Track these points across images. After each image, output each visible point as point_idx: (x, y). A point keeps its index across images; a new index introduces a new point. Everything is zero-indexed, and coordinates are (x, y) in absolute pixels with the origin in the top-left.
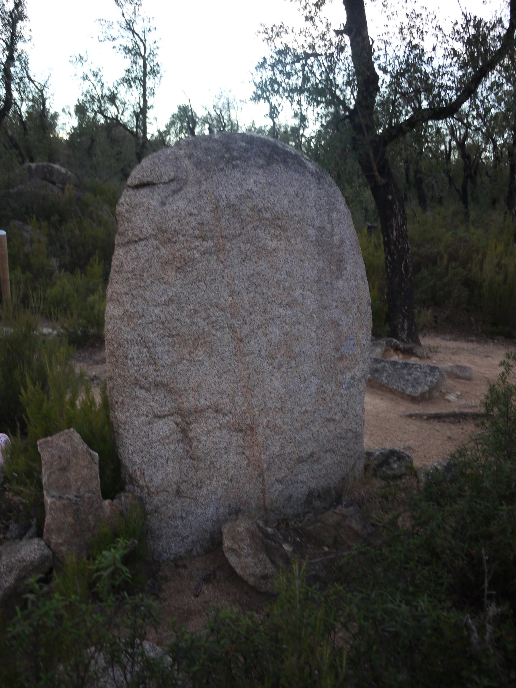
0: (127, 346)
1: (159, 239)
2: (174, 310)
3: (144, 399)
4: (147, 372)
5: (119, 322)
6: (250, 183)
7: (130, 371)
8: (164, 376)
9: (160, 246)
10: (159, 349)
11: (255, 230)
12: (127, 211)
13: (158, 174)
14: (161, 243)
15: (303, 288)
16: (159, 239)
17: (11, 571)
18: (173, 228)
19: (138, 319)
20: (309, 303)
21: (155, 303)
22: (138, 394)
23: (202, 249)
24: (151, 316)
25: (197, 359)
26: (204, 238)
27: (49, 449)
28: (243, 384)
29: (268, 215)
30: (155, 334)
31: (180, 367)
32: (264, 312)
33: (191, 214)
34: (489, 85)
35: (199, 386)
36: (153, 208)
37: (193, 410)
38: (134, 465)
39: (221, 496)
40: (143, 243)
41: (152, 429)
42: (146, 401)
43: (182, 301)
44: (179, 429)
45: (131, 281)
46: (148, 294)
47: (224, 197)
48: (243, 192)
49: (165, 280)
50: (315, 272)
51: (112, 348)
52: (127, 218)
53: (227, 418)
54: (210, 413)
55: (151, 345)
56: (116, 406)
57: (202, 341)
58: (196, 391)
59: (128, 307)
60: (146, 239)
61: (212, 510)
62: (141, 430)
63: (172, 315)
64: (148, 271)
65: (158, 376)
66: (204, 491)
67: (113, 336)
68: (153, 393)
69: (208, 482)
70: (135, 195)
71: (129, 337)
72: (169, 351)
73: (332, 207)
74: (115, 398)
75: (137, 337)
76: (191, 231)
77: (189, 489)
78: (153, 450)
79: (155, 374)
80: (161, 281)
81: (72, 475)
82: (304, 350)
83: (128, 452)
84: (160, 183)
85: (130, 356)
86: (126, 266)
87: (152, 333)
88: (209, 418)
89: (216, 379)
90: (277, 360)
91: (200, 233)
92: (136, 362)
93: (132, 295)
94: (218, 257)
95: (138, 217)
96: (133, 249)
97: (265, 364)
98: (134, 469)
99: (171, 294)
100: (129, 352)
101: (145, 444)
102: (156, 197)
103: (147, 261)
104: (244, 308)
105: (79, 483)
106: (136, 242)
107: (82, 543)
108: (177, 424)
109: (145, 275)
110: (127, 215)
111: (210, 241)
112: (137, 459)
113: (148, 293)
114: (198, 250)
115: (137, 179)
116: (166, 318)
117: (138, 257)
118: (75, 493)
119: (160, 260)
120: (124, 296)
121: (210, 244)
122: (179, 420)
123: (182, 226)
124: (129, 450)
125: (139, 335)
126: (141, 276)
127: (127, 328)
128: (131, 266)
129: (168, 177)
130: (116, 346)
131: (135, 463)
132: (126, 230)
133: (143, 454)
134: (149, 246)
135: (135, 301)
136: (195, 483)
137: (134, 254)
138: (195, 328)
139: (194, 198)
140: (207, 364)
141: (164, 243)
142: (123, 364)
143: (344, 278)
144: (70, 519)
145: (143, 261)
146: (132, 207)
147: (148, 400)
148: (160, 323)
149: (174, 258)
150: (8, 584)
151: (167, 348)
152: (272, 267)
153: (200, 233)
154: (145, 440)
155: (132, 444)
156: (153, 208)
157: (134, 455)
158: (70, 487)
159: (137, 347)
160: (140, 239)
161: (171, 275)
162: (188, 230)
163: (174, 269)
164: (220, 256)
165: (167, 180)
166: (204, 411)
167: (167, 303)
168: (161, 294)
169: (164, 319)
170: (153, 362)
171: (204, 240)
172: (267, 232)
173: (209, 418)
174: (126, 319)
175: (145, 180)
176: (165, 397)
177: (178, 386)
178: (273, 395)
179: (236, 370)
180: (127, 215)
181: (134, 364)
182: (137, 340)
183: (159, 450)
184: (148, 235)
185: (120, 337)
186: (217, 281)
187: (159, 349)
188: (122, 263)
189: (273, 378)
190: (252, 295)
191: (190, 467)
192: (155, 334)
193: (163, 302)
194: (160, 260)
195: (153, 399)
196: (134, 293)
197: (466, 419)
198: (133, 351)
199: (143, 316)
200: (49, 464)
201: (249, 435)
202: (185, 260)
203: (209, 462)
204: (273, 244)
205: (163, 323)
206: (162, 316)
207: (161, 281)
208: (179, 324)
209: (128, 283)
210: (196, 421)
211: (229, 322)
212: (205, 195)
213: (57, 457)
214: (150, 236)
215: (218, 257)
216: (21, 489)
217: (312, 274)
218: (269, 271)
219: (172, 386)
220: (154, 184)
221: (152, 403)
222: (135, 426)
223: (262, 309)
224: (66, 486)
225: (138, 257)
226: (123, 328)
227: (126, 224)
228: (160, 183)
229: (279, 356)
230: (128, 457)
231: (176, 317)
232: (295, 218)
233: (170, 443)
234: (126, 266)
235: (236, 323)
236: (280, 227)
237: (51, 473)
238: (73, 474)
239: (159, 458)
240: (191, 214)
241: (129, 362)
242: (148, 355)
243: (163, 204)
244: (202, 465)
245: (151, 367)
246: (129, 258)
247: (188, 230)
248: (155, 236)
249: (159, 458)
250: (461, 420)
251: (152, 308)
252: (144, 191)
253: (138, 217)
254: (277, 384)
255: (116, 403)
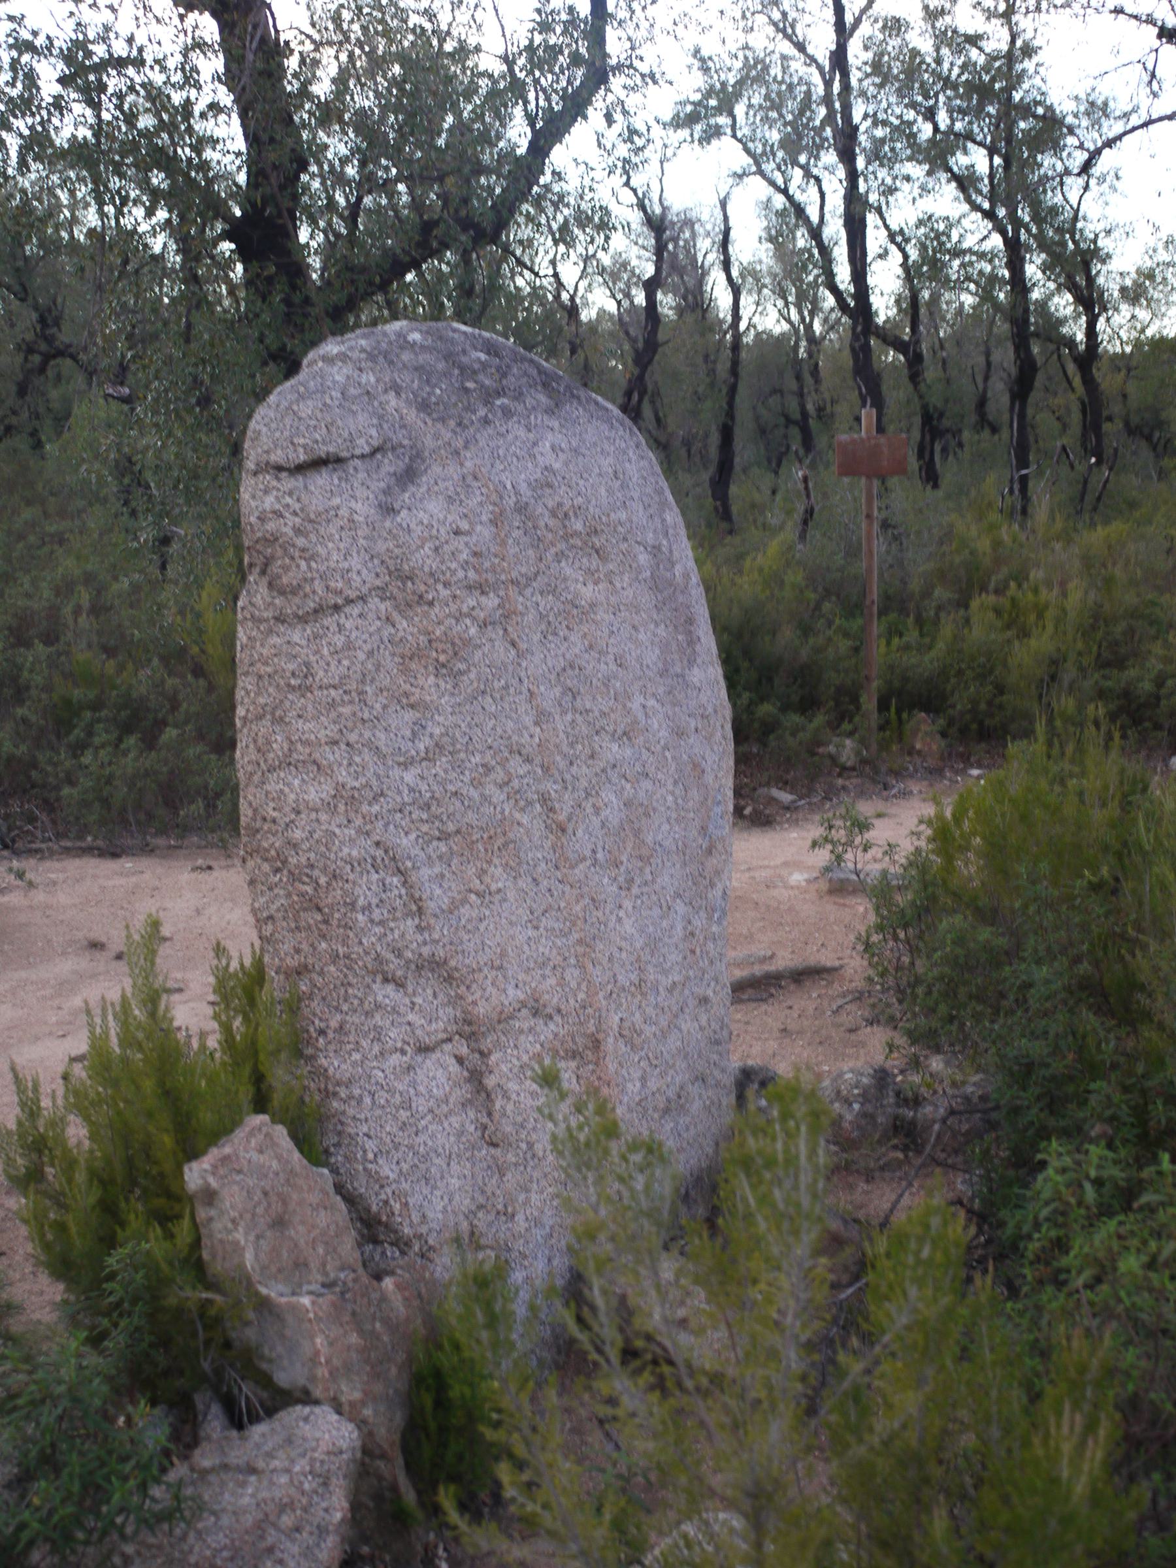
0: (351, 877)
1: (393, 598)
2: (446, 771)
3: (394, 1009)
4: (403, 935)
5: (323, 817)
6: (545, 456)
7: (364, 941)
8: (437, 942)
9: (396, 616)
10: (425, 872)
11: (559, 562)
12: (298, 531)
13: (346, 434)
14: (396, 607)
15: (643, 691)
16: (393, 598)
17: (325, 1484)
18: (426, 569)
19: (370, 804)
20: (656, 726)
21: (402, 759)
22: (380, 998)
23: (482, 615)
24: (399, 792)
25: (494, 887)
26: (482, 588)
27: (238, 1178)
28: (576, 936)
29: (578, 526)
30: (413, 836)
31: (465, 911)
32: (592, 757)
33: (457, 532)
34: (232, 97)
35: (503, 955)
36: (361, 519)
37: (495, 1016)
38: (382, 1187)
39: (552, 1227)
40: (355, 610)
41: (414, 1084)
42: (399, 1014)
43: (458, 746)
44: (466, 1074)
45: (341, 709)
46: (382, 738)
47: (509, 486)
48: (539, 471)
49: (412, 699)
50: (657, 651)
51: (309, 889)
52: (303, 550)
53: (552, 1026)
54: (525, 1021)
55: (409, 864)
56: (321, 1040)
57: (499, 842)
58: (501, 968)
59: (342, 775)
60: (362, 598)
61: (540, 1266)
62: (391, 1091)
63: (442, 783)
64: (373, 680)
65: (425, 943)
66: (520, 1223)
67: (312, 855)
68: (410, 990)
69: (522, 1197)
70: (306, 487)
71: (355, 853)
72: (442, 876)
73: (663, 505)
74: (317, 1022)
75: (372, 851)
76: (461, 574)
77: (490, 1224)
78: (421, 1139)
79: (420, 938)
80: (404, 701)
81: (298, 1232)
82: (660, 837)
83: (365, 1159)
84: (353, 456)
85: (361, 902)
86: (321, 673)
87: (406, 834)
88: (521, 1031)
89: (531, 933)
90: (622, 869)
91: (477, 577)
92: (377, 915)
93: (348, 744)
94: (505, 630)
95: (330, 545)
96: (334, 628)
97: (606, 880)
98: (383, 1197)
99: (437, 731)
100: (358, 891)
101: (403, 1127)
102: (361, 493)
103: (370, 654)
104: (561, 753)
105: (321, 1251)
106: (337, 608)
107: (391, 1392)
108: (460, 1060)
109: (368, 688)
110: (301, 542)
111: (492, 595)
112: (387, 1170)
113: (382, 736)
114: (474, 619)
115: (301, 450)
116: (433, 792)
117: (349, 646)
118: (320, 1278)
119: (399, 651)
120: (327, 749)
121: (491, 601)
122: (464, 1050)
123: (442, 562)
124: (365, 1151)
125: (378, 844)
126: (361, 693)
127: (346, 831)
128: (336, 671)
129: (367, 442)
130: (323, 880)
131: (382, 1183)
132: (306, 580)
133: (400, 1155)
134: (371, 616)
135: (357, 759)
136: (500, 1207)
137: (339, 640)
138: (487, 810)
139: (458, 494)
140: (511, 895)
141: (406, 607)
142: (346, 926)
143: (699, 661)
144: (354, 1338)
145: (361, 656)
146: (311, 521)
147: (402, 1010)
148: (421, 808)
149: (430, 641)
150: (338, 1516)
151: (437, 870)
152: (591, 647)
153: (477, 577)
154: (404, 1115)
155: (372, 1133)
156: (361, 519)
157: (380, 1162)
158: (306, 1265)
159: (375, 877)
160: (349, 601)
161: (429, 685)
162: (454, 572)
163: (430, 668)
164: (510, 629)
165: (367, 450)
166: (511, 1017)
167: (431, 755)
168: (408, 733)
169: (428, 795)
170: (414, 908)
171: (483, 593)
172: (577, 564)
173: (521, 1031)
174: (341, 808)
175: (322, 451)
176: (435, 995)
177: (467, 961)
178: (624, 955)
179: (563, 905)
180: (301, 542)
181: (372, 921)
182: (374, 858)
183: (433, 1136)
184: (364, 590)
185: (332, 856)
186: (512, 690)
187: (425, 872)
188: (307, 664)
189: (622, 914)
190: (569, 717)
191: (489, 1167)
192: (413, 836)
193: (423, 755)
194: (399, 651)
195: (413, 1003)
196: (353, 737)
197: (780, 987)
198: (365, 889)
199: (382, 794)
200: (248, 1216)
201: (589, 1062)
202: (453, 644)
203: (524, 1146)
204: (588, 592)
205: (427, 806)
206: (424, 787)
207: (404, 701)
208: (458, 804)
209: (333, 714)
210: (497, 1044)
211: (542, 787)
212: (475, 484)
213: (259, 1193)
214: (370, 590)
215: (505, 630)
216: (204, 1295)
217: (652, 657)
218: (587, 656)
219: (453, 963)
220: (339, 460)
221: (411, 1017)
222: (377, 1083)
223: (588, 751)
224: (297, 1265)
225: (349, 646)
226: (337, 831)
227: (303, 564)
228: (353, 456)
229: (624, 859)
230: (365, 1169)
231: (451, 788)
232: (620, 529)
233: (451, 1112)
234: (321, 673)
235: (551, 787)
236: (597, 552)
237: (258, 1237)
238: (301, 1228)
239: (432, 1155)
240: (457, 532)
241: (360, 917)
242: (403, 891)
243: (389, 510)
244: (510, 1157)
245: (409, 922)
246: (325, 651)
247: (454, 572)
248: (382, 592)
249: (432, 1155)
250: (773, 991)
251: (396, 772)
252: (322, 480)
253: (330, 545)
254: (628, 927)
255: (322, 1032)
